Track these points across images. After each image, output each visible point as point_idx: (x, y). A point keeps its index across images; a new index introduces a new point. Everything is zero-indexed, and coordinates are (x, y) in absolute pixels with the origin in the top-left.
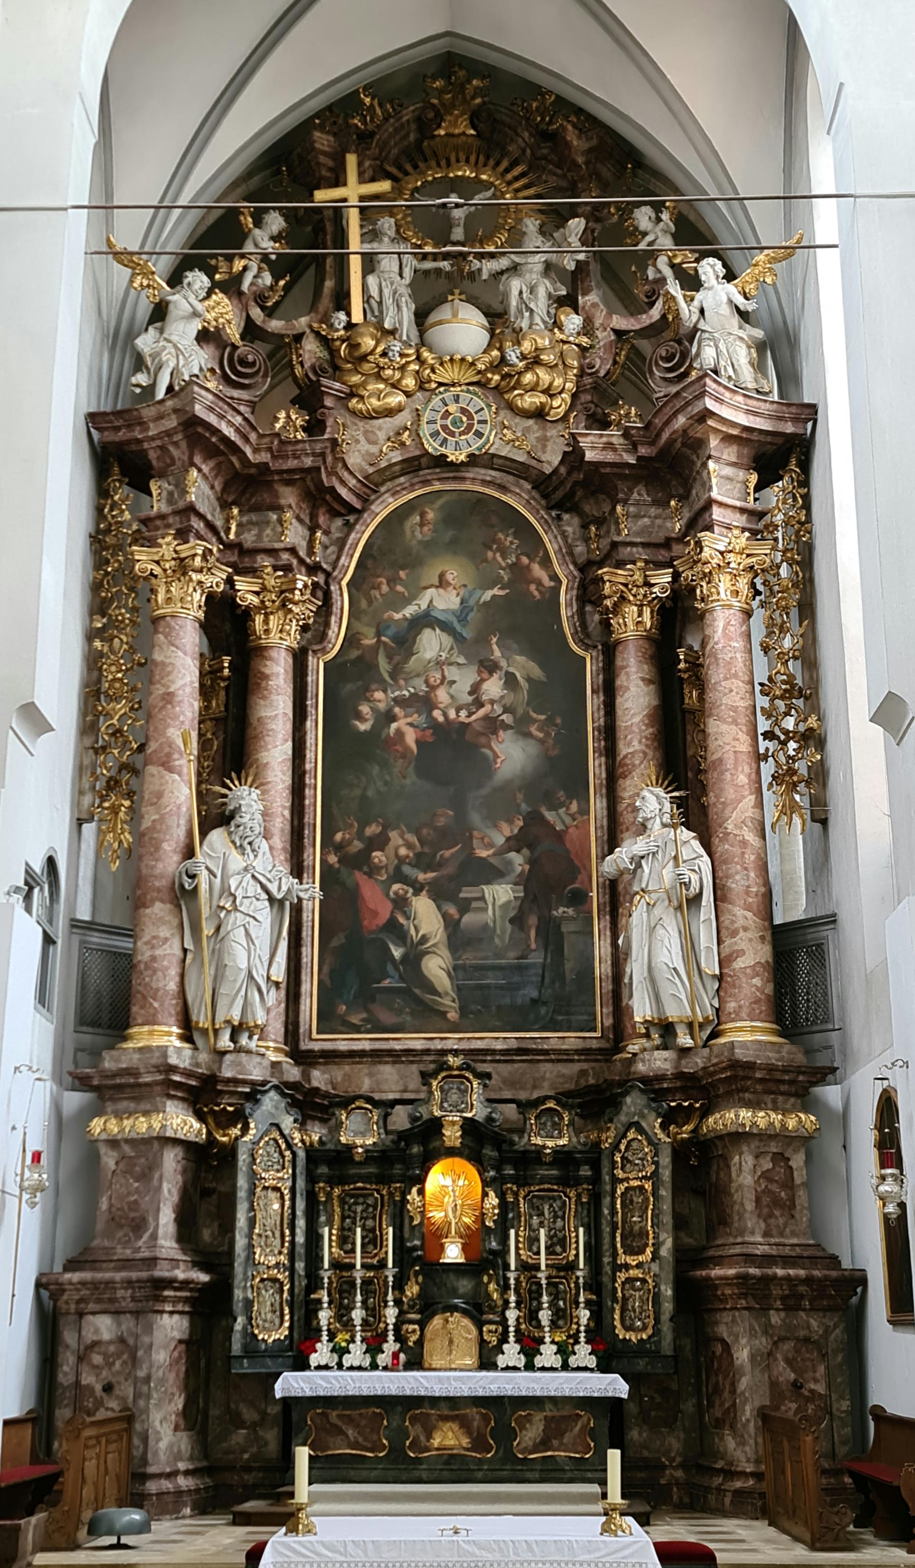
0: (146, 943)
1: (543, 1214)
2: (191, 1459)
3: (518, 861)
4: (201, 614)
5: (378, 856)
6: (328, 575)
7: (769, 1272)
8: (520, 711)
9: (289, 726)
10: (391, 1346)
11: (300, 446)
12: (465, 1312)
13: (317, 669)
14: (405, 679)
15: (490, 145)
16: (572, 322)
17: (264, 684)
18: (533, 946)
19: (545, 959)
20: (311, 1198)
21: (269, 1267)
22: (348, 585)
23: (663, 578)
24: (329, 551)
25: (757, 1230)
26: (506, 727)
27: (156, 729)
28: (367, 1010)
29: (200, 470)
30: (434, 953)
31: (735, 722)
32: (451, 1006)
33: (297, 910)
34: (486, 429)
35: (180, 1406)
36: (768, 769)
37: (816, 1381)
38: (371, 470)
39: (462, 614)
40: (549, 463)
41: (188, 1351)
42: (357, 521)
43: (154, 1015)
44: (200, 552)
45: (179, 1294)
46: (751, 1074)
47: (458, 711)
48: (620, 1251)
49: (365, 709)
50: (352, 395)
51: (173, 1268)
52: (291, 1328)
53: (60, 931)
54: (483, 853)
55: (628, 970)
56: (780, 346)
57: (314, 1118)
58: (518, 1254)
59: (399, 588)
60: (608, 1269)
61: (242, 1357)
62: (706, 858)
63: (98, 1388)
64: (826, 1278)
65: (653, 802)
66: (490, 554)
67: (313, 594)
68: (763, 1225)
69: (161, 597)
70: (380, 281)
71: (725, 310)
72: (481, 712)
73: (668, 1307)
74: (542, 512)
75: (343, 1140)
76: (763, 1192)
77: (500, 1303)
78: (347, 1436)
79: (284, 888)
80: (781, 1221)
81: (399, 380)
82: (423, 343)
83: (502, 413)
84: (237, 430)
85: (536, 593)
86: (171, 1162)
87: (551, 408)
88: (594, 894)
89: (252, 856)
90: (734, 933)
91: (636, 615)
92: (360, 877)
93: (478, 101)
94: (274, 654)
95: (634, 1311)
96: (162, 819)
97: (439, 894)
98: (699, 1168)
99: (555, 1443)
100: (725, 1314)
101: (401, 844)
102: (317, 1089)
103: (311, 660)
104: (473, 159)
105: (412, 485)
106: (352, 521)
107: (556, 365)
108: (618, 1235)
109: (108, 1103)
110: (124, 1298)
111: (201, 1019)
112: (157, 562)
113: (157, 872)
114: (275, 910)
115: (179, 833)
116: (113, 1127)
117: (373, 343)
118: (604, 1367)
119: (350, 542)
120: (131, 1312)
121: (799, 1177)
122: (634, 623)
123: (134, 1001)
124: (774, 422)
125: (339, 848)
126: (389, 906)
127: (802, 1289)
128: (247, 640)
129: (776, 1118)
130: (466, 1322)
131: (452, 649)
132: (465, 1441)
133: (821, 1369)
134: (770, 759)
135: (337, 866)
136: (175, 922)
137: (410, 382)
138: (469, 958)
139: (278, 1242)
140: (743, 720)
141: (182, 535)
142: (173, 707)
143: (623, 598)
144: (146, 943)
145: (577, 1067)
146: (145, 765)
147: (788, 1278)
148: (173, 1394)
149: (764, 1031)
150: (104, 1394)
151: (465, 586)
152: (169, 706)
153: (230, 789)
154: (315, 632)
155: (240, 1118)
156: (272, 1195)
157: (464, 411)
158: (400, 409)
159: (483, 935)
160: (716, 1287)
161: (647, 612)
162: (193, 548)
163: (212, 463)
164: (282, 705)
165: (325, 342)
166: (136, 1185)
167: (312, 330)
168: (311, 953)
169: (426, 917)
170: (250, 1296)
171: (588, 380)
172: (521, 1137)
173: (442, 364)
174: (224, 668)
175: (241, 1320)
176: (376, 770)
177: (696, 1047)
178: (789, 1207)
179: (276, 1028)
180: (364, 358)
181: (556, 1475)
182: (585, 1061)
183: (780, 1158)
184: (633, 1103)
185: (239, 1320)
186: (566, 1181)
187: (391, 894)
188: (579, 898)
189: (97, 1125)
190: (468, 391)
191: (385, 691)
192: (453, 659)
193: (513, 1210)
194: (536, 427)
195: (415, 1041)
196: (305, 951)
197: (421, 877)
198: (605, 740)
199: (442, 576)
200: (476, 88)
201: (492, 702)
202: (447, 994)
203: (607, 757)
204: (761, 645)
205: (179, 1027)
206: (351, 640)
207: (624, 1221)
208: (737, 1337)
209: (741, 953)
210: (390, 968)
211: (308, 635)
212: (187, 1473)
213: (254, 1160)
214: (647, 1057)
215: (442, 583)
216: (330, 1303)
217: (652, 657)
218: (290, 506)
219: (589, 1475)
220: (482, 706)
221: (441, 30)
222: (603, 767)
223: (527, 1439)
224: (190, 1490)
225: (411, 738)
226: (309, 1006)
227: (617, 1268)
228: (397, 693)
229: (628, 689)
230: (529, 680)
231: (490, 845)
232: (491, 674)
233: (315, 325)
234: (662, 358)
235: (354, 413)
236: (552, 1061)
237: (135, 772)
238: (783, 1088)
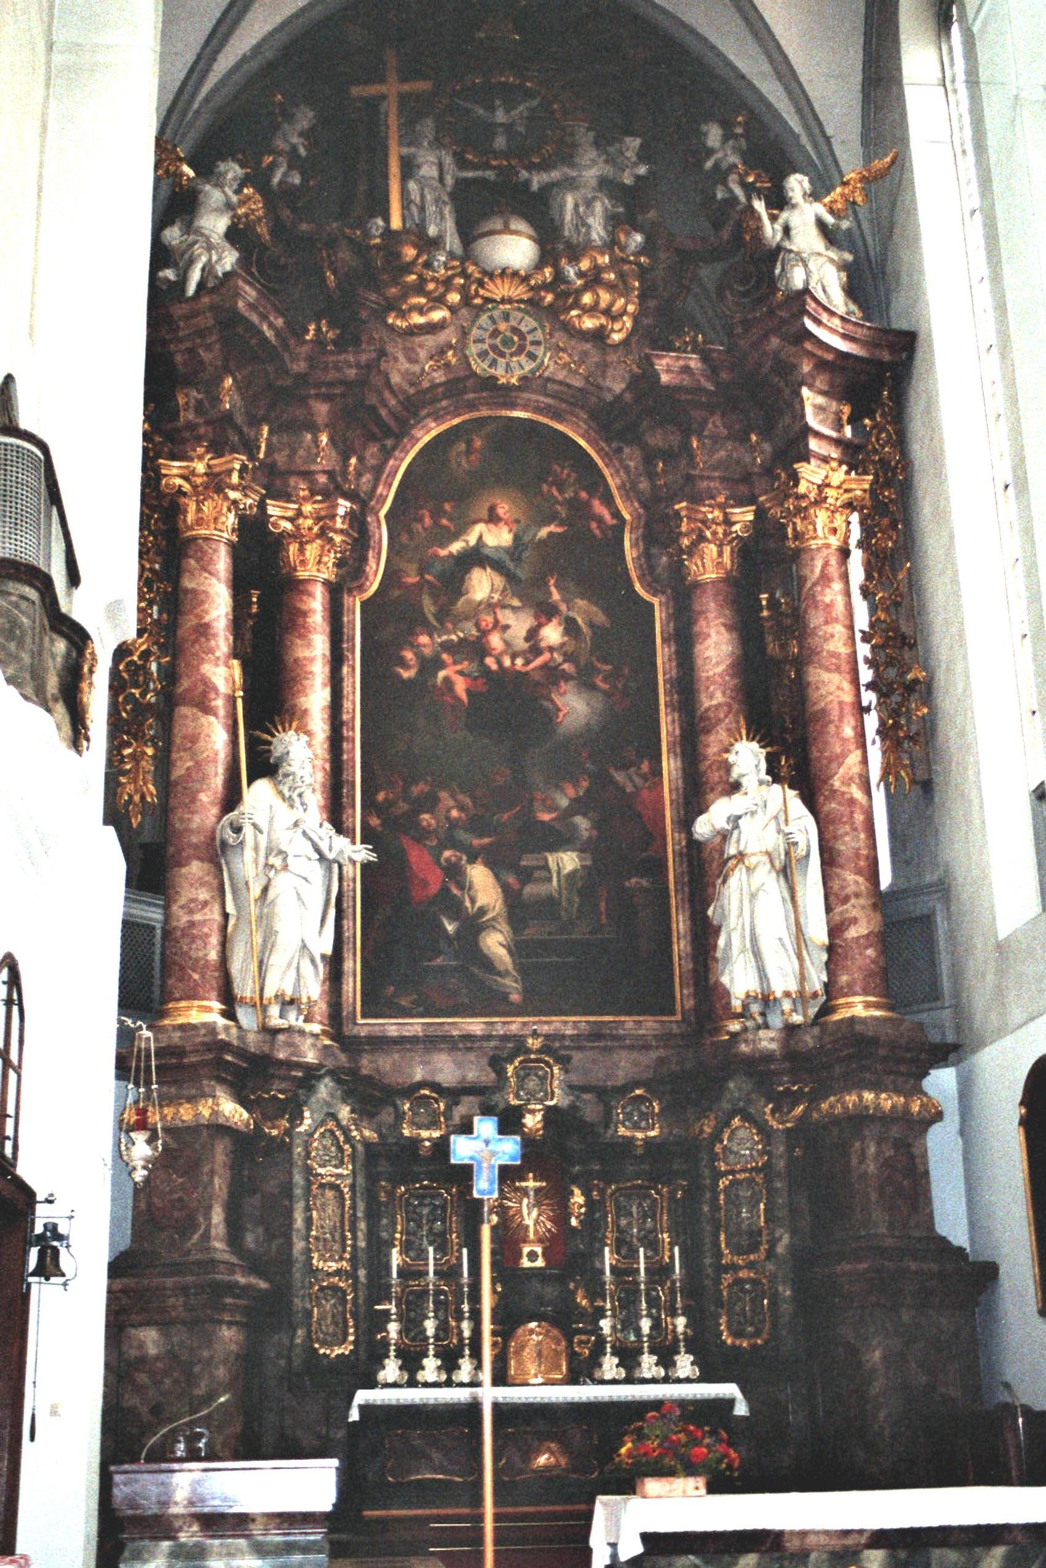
0: (182, 907)
1: (631, 1214)
13: (354, 606)
14: (455, 624)
17: (300, 621)
18: (604, 920)
22: (386, 516)
23: (744, 515)
26: (567, 677)
27: (187, 665)
30: (494, 928)
31: (838, 670)
32: (513, 987)
34: (540, 351)
38: (412, 391)
40: (609, 390)
43: (194, 989)
44: (237, 467)
47: (514, 657)
49: (409, 655)
54: (546, 817)
56: (875, 267)
63: (144, 1410)
65: (748, 758)
69: (190, 518)
70: (417, 191)
75: (406, 1132)
81: (443, 295)
85: (597, 532)
86: (221, 1153)
87: (612, 330)
89: (301, 809)
90: (846, 900)
91: (715, 554)
92: (406, 842)
96: (198, 764)
101: (452, 808)
103: (347, 600)
110: (174, 1307)
111: (245, 987)
113: (194, 826)
115: (217, 780)
119: (387, 470)
120: (184, 1323)
122: (711, 564)
131: (504, 590)
135: (380, 829)
136: (215, 883)
137: (454, 298)
138: (532, 932)
140: (845, 667)
142: (208, 640)
143: (702, 538)
144: (182, 907)
145: (654, 1055)
149: (876, 1006)
151: (517, 521)
152: (203, 639)
156: (330, 1194)
157: (515, 330)
158: (441, 326)
159: (548, 906)
161: (727, 550)
162: (231, 462)
169: (483, 886)
170: (308, 1306)
174: (252, 603)
177: (805, 1024)
180: (408, 268)
187: (442, 860)
190: (519, 309)
194: (593, 352)
196: (347, 924)
197: (476, 842)
199: (492, 509)
201: (551, 649)
205: (222, 1002)
206: (391, 576)
209: (855, 921)
210: (443, 945)
214: (751, 1037)
215: (493, 518)
225: (460, 686)
226: (352, 987)
228: (445, 638)
229: (709, 635)
230: (591, 625)
231: (553, 808)
232: (550, 620)
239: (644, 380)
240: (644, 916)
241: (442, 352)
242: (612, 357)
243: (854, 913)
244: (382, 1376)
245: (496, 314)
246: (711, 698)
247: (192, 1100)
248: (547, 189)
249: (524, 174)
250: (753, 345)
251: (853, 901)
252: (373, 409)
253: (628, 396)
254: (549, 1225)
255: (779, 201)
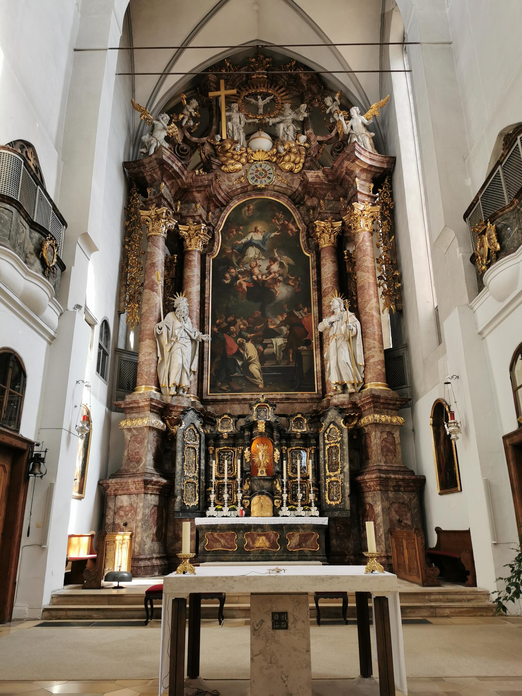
2: (159, 553)
3: (285, 329)
4: (165, 236)
5: (232, 328)
6: (214, 228)
7: (388, 476)
8: (285, 276)
9: (199, 279)
10: (239, 508)
11: (203, 177)
12: (267, 495)
14: (243, 265)
15: (272, 81)
16: (303, 138)
17: (189, 264)
18: (291, 360)
19: (296, 365)
20: (207, 452)
21: (190, 478)
23: (339, 223)
24: (214, 220)
25: (382, 461)
26: (280, 281)
28: (229, 384)
29: (165, 184)
33: (202, 343)
34: (271, 176)
35: (155, 532)
36: (381, 290)
37: (407, 519)
39: (264, 241)
40: (295, 188)
41: (158, 510)
42: (224, 209)
45: (154, 487)
46: (379, 401)
48: (327, 470)
49: (227, 275)
50: (222, 165)
51: (152, 476)
52: (199, 501)
53: (110, 351)
54: (272, 327)
55: (328, 366)
56: (382, 137)
57: (208, 424)
58: (287, 473)
59: (240, 232)
60: (323, 478)
61: (180, 512)
62: (358, 322)
63: (122, 524)
64: (410, 479)
65: (337, 302)
66: (273, 220)
67: (208, 233)
68: (384, 459)
69: (150, 229)
70: (233, 123)
71: (361, 126)
72: (271, 276)
73: (347, 491)
74: (292, 205)
76: (384, 446)
77: (281, 491)
78: (221, 543)
79: (197, 335)
80: (391, 457)
81: (240, 159)
82: (248, 146)
83: (277, 171)
84: (179, 168)
85: (291, 234)
88: (314, 341)
90: (370, 349)
93: (268, 65)
94: (193, 253)
95: (333, 493)
96: (150, 309)
97: (255, 342)
98: (358, 441)
99: (304, 545)
100: (370, 493)
101: (241, 324)
102: (210, 412)
104: (266, 86)
105: (245, 196)
106: (222, 209)
107: (297, 153)
108: (327, 465)
109: (128, 415)
111: (163, 382)
112: (149, 217)
114: (193, 345)
116: (129, 423)
117: (230, 146)
118: (321, 515)
121: (398, 441)
122: (326, 242)
123: (138, 377)
124: (380, 164)
125: (218, 326)
126: (237, 346)
127: (400, 483)
128: (184, 249)
129: (388, 418)
130: (268, 498)
131: (260, 254)
132: (268, 544)
133: (409, 515)
134: (381, 287)
136: (155, 347)
137: (244, 160)
138: (267, 364)
139: (194, 468)
141: (159, 206)
145: (308, 405)
146: (144, 289)
147: (395, 479)
148: (151, 526)
149: (382, 385)
150: (124, 527)
153: (175, 298)
154: (208, 247)
155: (179, 422)
156: (191, 450)
157: (263, 170)
159: (273, 356)
160: (366, 482)
163: (170, 182)
164: (196, 271)
165: (213, 146)
166: (138, 445)
167: (208, 142)
168: (207, 363)
169: (251, 350)
170: (183, 488)
171: (309, 159)
172: (288, 428)
173: (255, 152)
175: (179, 498)
176: (232, 297)
178: (394, 452)
179: (194, 389)
180: (227, 151)
181: (304, 557)
182: (311, 402)
183: (390, 433)
184: (332, 414)
185: (178, 497)
186: (306, 446)
188: (308, 343)
189: (123, 423)
190: (265, 163)
191: (235, 269)
192: (260, 257)
193: (285, 456)
194: (290, 176)
195: (247, 396)
196: (205, 363)
197: (249, 336)
198: (317, 285)
199: (256, 228)
200: (267, 61)
201: (275, 273)
202: (259, 378)
203: (318, 291)
204: (377, 245)
206: (222, 251)
207: (329, 460)
208: (376, 501)
209: (373, 356)
210: (237, 369)
211: (206, 249)
212: (157, 558)
213: (184, 436)
215: (256, 231)
216: (215, 492)
217: (335, 253)
218: (200, 201)
219: (318, 558)
220: (271, 274)
221: (255, 39)
222: (317, 295)
223: (292, 543)
224: (158, 565)
225: (244, 285)
227: (326, 477)
230: (288, 264)
232: (274, 263)
233: (209, 140)
234: (336, 148)
235: (223, 171)
236: (299, 403)
237: (140, 293)
238: (391, 407)
239: (305, 183)
240: (298, 369)
241: (240, 178)
242: (296, 177)
243: (373, 354)
244: (208, 513)
245: (258, 165)
246: (327, 284)
247: (142, 418)
248: (274, 125)
249: (267, 120)
250: (340, 165)
251: (373, 349)
252: (215, 196)
253: (300, 189)
254: (268, 461)
255: (349, 118)
